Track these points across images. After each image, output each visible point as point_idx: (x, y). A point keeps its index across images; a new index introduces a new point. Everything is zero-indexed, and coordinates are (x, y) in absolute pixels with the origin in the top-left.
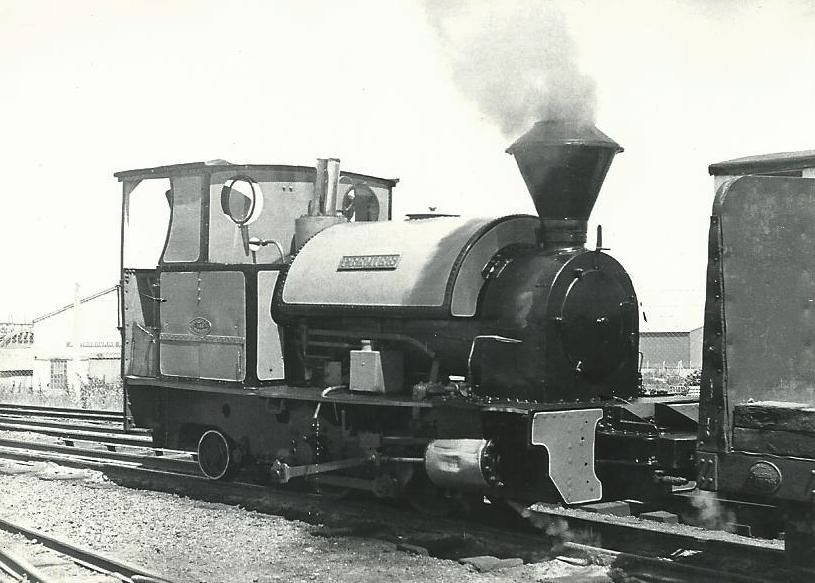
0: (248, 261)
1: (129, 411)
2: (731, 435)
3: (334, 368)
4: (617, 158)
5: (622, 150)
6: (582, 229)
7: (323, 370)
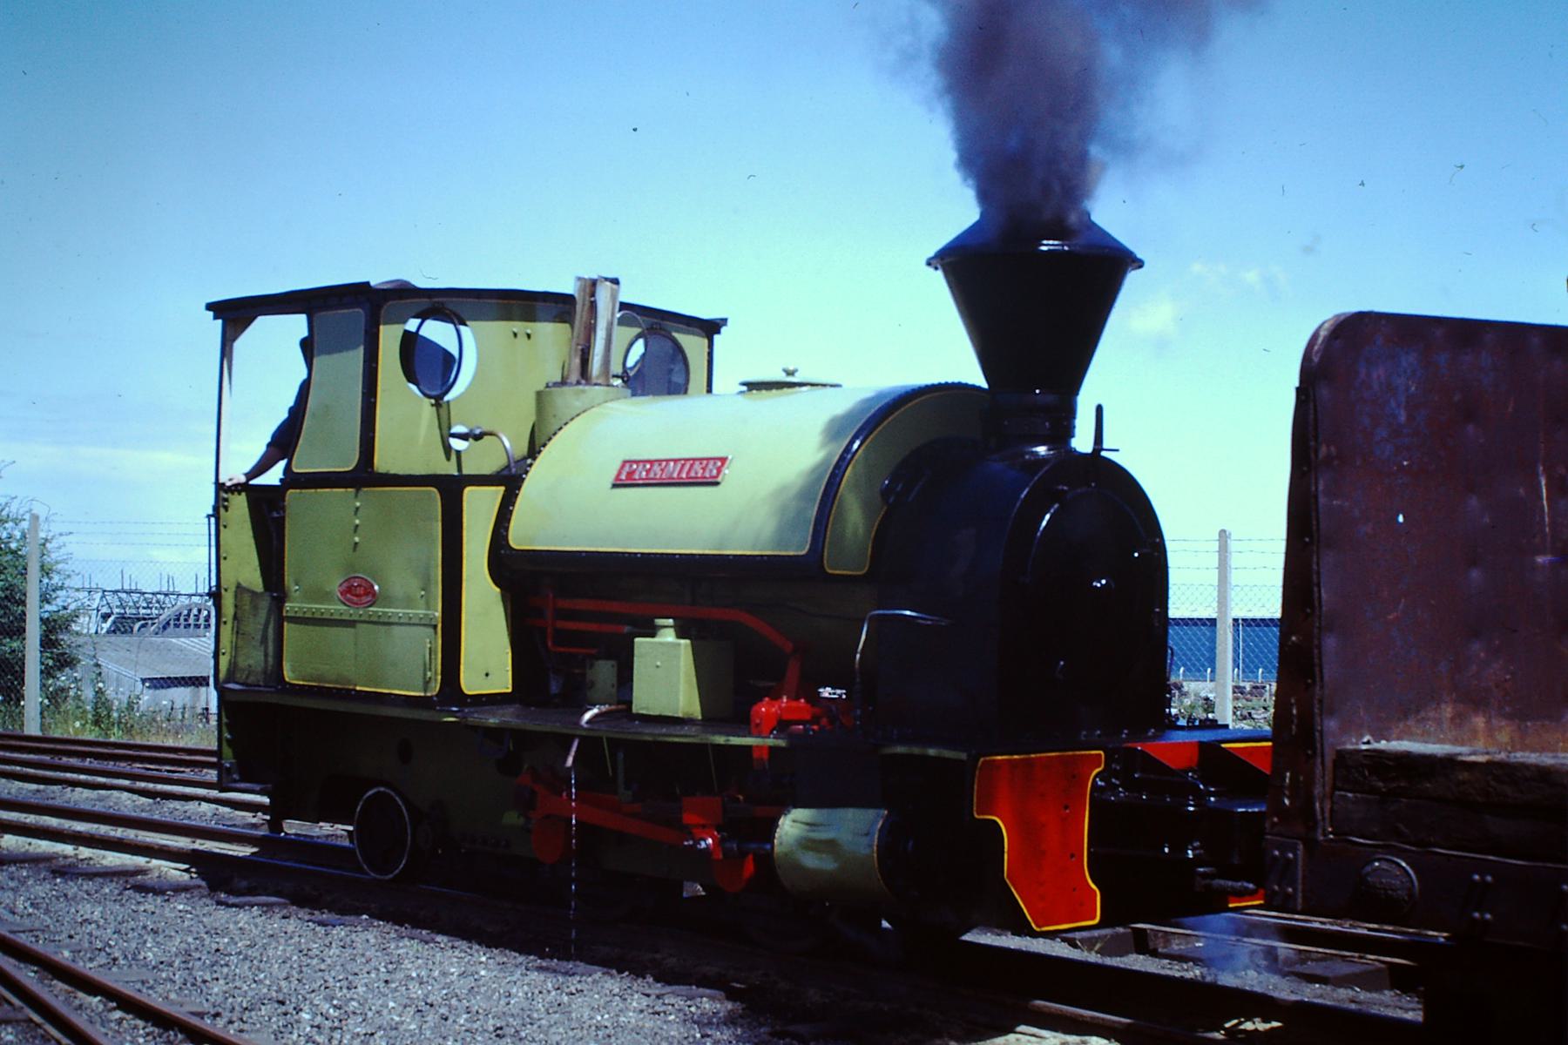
0: (450, 469)
1: (227, 751)
2: (1328, 806)
3: (604, 671)
4: (1132, 278)
5: (1139, 264)
6: (1070, 412)
7: (584, 675)
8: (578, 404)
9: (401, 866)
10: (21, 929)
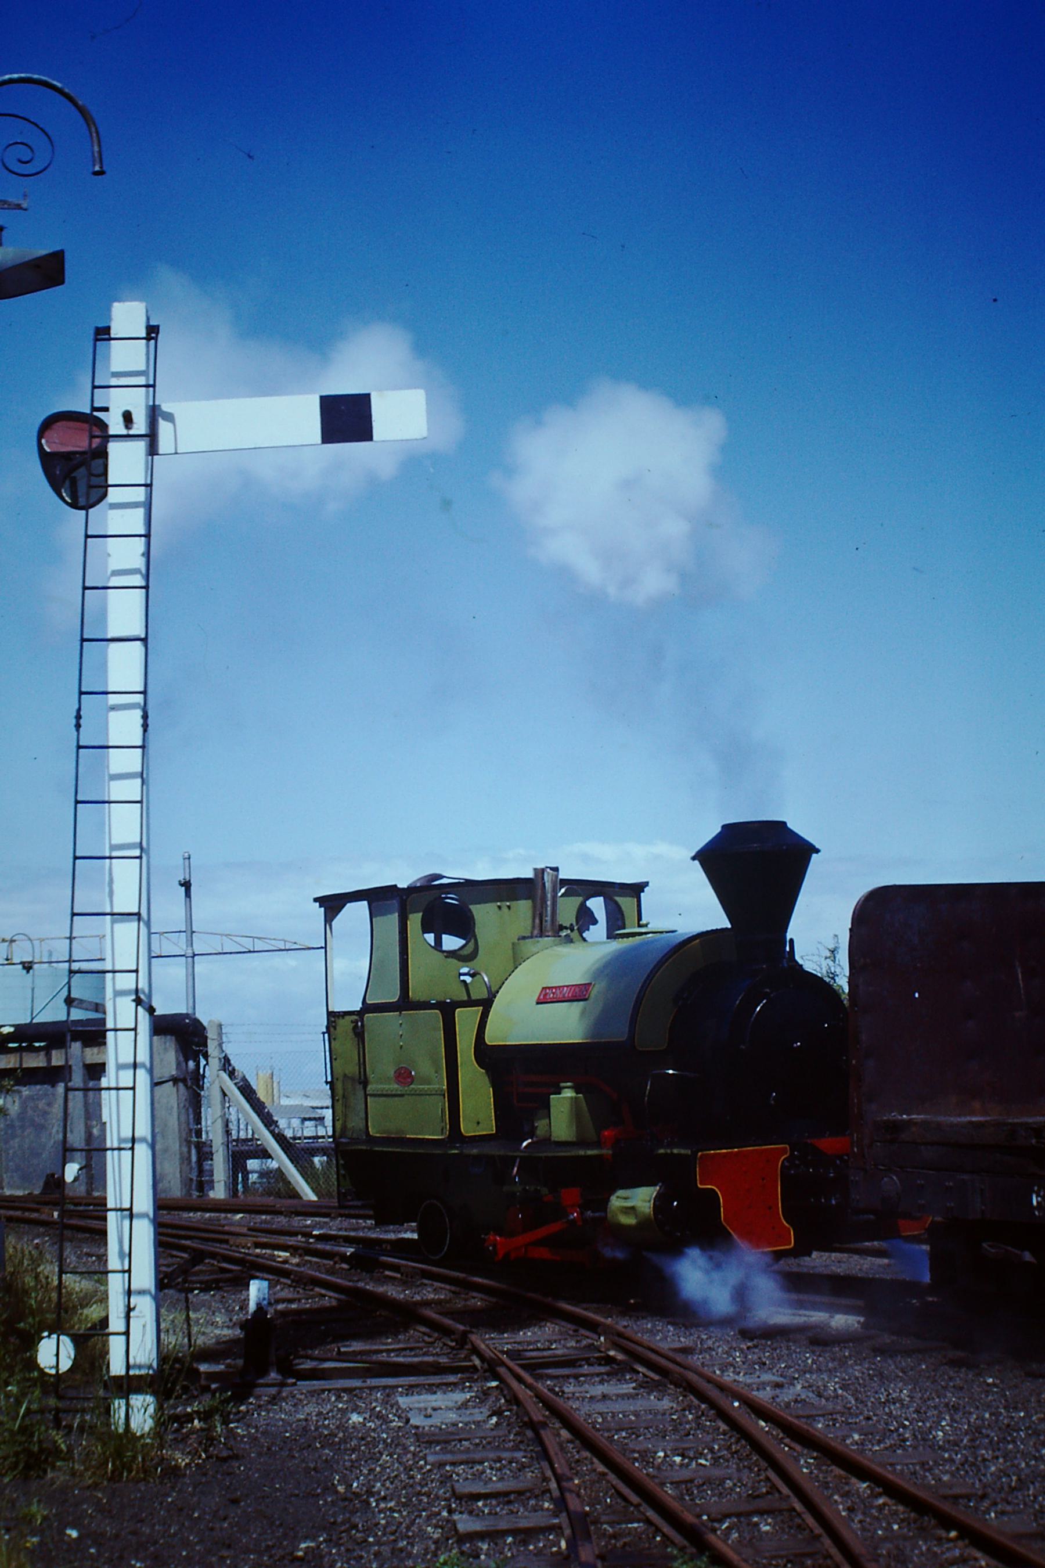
5: (817, 851)
8: (535, 950)
9: (448, 1242)
10: (820, 1412)
